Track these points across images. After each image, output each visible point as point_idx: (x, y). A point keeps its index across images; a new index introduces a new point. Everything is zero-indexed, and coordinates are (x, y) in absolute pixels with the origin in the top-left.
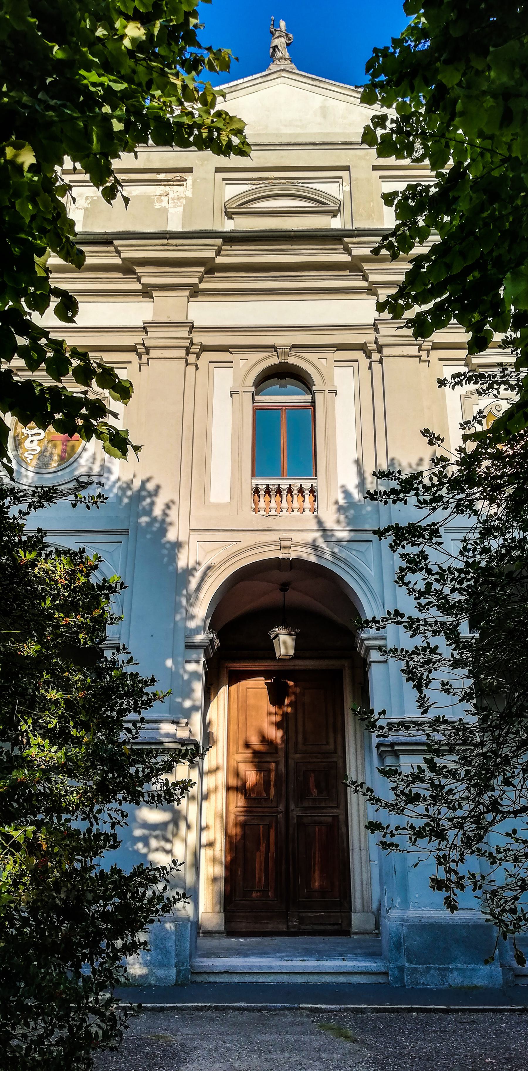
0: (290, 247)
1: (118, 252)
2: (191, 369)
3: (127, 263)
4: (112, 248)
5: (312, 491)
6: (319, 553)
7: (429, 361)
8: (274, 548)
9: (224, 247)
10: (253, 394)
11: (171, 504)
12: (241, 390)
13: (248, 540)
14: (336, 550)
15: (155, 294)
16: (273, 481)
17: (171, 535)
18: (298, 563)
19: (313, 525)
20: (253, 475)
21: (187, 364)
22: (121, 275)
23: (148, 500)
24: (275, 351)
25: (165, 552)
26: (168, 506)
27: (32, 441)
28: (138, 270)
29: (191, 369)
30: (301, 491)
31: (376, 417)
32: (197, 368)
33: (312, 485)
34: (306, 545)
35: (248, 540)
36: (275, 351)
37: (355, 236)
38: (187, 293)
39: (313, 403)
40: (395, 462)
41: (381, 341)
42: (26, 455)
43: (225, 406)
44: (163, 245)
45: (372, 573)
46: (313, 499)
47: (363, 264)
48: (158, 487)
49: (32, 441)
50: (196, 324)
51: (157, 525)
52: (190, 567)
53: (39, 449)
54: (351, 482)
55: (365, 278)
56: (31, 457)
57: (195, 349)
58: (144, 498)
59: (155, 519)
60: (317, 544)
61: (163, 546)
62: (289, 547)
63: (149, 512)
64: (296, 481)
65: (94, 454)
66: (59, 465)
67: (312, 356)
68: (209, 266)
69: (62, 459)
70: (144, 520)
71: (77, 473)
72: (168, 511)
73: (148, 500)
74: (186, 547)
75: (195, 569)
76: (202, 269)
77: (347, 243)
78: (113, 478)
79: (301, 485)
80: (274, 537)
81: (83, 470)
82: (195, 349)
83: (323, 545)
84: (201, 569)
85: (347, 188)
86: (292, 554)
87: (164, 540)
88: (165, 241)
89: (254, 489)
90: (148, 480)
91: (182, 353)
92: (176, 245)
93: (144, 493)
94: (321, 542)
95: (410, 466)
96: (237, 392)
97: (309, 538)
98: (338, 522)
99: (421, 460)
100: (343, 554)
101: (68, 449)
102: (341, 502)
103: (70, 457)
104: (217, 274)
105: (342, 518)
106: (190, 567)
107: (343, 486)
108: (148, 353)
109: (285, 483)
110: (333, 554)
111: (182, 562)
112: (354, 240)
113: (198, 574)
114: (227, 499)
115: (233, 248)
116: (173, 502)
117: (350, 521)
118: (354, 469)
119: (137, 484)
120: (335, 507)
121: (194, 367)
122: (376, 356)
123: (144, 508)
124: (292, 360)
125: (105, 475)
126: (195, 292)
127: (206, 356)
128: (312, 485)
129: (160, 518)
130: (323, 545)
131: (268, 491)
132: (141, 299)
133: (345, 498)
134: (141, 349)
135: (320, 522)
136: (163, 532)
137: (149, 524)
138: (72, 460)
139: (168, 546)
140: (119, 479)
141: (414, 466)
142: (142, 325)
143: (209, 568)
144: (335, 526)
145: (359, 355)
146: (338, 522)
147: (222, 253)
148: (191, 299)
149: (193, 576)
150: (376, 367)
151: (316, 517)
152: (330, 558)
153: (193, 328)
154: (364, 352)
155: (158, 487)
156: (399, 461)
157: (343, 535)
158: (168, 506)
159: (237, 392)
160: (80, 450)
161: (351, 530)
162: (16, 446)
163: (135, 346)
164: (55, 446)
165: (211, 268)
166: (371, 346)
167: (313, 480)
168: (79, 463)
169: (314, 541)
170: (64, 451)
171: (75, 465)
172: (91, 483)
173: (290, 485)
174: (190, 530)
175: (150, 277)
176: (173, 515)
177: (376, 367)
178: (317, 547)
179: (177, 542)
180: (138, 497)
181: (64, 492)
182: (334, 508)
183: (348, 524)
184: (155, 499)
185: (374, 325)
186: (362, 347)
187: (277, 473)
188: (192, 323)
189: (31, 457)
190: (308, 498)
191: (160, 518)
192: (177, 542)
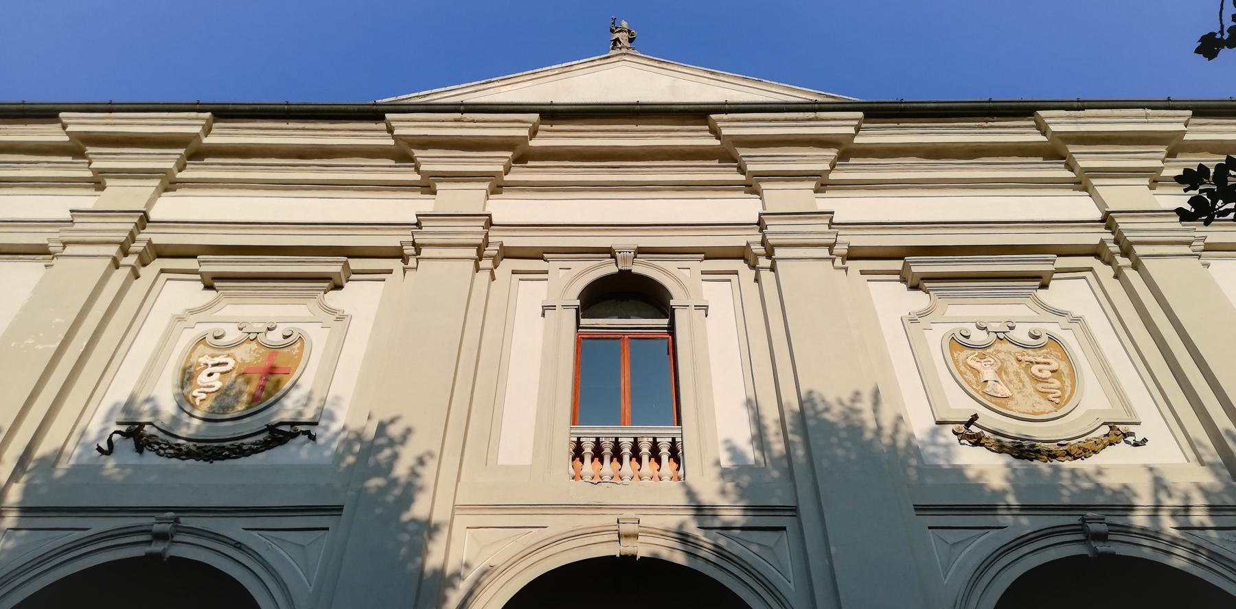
0: (633, 127)
1: (390, 130)
2: (484, 276)
3: (401, 143)
4: (382, 126)
5: (675, 454)
6: (690, 548)
7: (846, 269)
8: (606, 538)
9: (541, 127)
10: (577, 310)
11: (427, 459)
12: (558, 304)
13: (559, 524)
14: (722, 542)
15: (439, 186)
16: (607, 432)
17: (420, 509)
18: (654, 563)
19: (682, 500)
20: (574, 422)
21: (477, 269)
22: (392, 163)
23: (387, 452)
24: (613, 257)
25: (406, 537)
26: (421, 462)
27: (210, 375)
28: (417, 153)
29: (484, 276)
30: (655, 453)
31: (777, 340)
32: (493, 278)
33: (674, 439)
34: (665, 533)
35: (559, 524)
36: (613, 257)
37: (726, 112)
38: (486, 186)
39: (671, 329)
40: (815, 396)
41: (772, 240)
42: (195, 393)
43: (535, 326)
44: (456, 121)
45: (791, 586)
46: (675, 466)
47: (738, 149)
48: (409, 431)
49: (210, 375)
50: (495, 221)
51: (397, 492)
52: (449, 570)
53: (218, 385)
54: (742, 435)
55: (742, 170)
56: (204, 396)
57: (492, 250)
58: (381, 448)
59: (394, 482)
60: (685, 530)
61: (403, 527)
62: (636, 536)
63: (386, 470)
64: (646, 434)
65: (311, 392)
66: (247, 408)
67: (671, 265)
68: (519, 151)
69: (255, 399)
70: (375, 482)
71: (276, 420)
72: (420, 470)
73: (387, 452)
74: (446, 530)
75: (457, 575)
76: (509, 154)
77: (715, 121)
78: (335, 427)
79: (655, 439)
80: (609, 519)
81: (286, 416)
82: (492, 250)
83: (699, 534)
84: (470, 576)
85: (702, 553)
86: (642, 549)
87: (406, 517)
88: (458, 115)
89: (574, 445)
90: (393, 421)
91: (473, 252)
92: (473, 121)
93: (382, 441)
94: (692, 528)
95: (841, 403)
96: (553, 307)
97: (672, 521)
98: (723, 492)
99: (857, 394)
100: (736, 549)
101: (269, 385)
102: (726, 463)
103: (270, 395)
104: (530, 163)
105: (729, 486)
106: (449, 570)
107: (727, 441)
108: (418, 252)
109: (626, 435)
110: (718, 550)
111: (434, 560)
112: (724, 116)
113: (463, 586)
114: (526, 460)
115: (555, 127)
116: (431, 455)
117: (742, 492)
118: (744, 415)
119: (371, 430)
120: (717, 470)
121: (488, 273)
122: (764, 262)
123: (378, 464)
124: (638, 269)
125: (322, 423)
126: (498, 186)
127: (508, 265)
128: (674, 439)
129: (403, 480)
130: (699, 534)
131: (598, 453)
132: (418, 195)
133: (732, 459)
134: (409, 250)
135: (690, 493)
136: (407, 500)
137: (382, 491)
138: (272, 399)
139: (412, 527)
140: (344, 428)
141: (848, 403)
142: (68, 216)
143: (485, 572)
144: (719, 501)
145: (739, 265)
146: (723, 492)
147: (539, 134)
148: (491, 197)
149: (454, 586)
150: (766, 276)
151: (684, 484)
152: (712, 558)
153: (492, 225)
154: (746, 261)
155: (409, 431)
156: (820, 395)
157: (733, 516)
158: (421, 462)
159: (553, 307)
160: (287, 385)
161: (746, 508)
162: (182, 382)
163: (401, 248)
164: (248, 382)
165: (523, 155)
166: (758, 249)
167: (674, 430)
168: (282, 406)
169: (681, 526)
170: (262, 388)
171: (275, 407)
172: (294, 435)
173: (636, 439)
174: (455, 507)
175: (432, 161)
176: (428, 474)
177: (766, 276)
178: (687, 535)
179: (428, 522)
180: (371, 448)
181: (245, 447)
182: (715, 471)
183: (741, 497)
184: (399, 448)
185: (758, 224)
186: (742, 254)
187: (616, 420)
188: (490, 215)
189: (204, 396)
190: (667, 466)
191: (403, 480)
192: (428, 522)
